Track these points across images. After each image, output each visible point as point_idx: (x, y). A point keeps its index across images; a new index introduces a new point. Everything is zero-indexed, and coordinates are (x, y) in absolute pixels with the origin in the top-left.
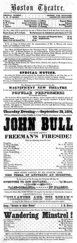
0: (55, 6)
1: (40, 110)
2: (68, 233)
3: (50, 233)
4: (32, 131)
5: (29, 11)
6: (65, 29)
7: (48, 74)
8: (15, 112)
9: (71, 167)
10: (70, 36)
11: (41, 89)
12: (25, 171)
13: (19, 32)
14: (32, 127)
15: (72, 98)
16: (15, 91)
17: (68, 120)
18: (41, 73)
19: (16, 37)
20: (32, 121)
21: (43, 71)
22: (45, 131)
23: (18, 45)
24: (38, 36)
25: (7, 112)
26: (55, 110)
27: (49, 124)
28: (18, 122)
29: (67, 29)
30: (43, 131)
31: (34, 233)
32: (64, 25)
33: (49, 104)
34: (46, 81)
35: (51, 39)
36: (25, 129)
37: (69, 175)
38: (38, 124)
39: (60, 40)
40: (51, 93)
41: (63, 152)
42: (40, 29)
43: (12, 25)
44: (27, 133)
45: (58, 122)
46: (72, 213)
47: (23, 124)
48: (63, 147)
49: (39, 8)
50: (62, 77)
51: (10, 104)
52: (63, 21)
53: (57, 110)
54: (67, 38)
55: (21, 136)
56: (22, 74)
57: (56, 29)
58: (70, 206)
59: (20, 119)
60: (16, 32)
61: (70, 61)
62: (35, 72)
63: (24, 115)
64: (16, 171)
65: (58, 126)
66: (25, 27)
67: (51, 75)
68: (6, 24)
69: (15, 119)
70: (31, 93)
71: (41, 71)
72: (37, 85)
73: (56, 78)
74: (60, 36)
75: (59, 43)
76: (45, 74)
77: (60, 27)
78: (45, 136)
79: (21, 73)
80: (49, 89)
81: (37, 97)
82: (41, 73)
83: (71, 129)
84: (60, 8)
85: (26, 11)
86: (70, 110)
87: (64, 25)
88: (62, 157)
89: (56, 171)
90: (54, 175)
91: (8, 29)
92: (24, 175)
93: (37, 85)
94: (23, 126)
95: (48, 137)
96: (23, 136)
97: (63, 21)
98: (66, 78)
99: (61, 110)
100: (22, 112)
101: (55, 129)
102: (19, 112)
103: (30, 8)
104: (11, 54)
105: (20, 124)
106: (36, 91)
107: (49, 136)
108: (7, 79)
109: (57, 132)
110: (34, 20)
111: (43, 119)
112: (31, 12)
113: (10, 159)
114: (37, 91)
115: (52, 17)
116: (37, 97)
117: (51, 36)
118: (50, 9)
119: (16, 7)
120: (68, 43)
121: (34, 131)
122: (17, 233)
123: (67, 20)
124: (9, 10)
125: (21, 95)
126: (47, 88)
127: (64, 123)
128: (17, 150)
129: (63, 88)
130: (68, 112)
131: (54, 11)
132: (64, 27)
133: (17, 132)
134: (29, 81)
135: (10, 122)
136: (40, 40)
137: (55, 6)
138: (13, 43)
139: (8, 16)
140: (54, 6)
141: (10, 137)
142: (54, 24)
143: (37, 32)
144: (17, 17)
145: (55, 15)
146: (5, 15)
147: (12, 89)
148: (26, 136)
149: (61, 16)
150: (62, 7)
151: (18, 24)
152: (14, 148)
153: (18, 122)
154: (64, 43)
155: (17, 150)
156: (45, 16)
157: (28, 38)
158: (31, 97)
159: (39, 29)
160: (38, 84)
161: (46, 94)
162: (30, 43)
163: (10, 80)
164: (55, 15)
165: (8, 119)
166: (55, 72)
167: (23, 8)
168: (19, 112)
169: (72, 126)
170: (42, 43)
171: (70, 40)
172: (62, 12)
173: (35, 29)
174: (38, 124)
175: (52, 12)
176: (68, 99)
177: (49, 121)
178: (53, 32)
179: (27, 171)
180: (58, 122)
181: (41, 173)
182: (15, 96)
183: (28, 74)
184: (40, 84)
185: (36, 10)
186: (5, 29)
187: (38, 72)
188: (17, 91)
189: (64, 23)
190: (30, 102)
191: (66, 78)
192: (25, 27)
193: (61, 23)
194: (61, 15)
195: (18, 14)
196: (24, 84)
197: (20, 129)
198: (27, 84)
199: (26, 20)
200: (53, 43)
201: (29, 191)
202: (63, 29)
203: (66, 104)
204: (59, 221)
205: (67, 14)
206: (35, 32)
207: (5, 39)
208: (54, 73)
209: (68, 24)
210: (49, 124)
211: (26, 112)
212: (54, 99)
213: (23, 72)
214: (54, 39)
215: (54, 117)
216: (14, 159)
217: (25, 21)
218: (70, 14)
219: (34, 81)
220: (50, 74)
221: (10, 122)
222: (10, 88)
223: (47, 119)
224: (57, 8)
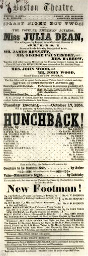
1: (50, 104)
5: (34, 12)
26: (62, 104)
39: (70, 93)
47: (7, 120)
49: (46, 8)
53: (64, 104)
58: (82, 241)
84: (69, 8)
85: (30, 12)
86: (81, 104)
118: (57, 9)
131: (62, 12)
136: (46, 94)
139: (9, 17)
145: (64, 16)
149: (70, 17)
167: (27, 7)
171: (80, 94)
172: (72, 12)
180: (35, 36)
185: (41, 10)
204: (70, 155)
205: (77, 15)
224: (65, 9)
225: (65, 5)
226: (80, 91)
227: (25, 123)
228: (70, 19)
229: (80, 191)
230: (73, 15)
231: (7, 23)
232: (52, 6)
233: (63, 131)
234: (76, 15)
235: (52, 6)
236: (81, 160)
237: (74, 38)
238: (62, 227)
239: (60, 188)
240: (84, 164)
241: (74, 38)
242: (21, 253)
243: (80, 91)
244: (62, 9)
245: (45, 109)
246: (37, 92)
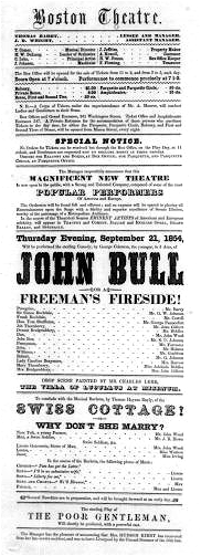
2: (172, 497)
3: (127, 496)
4: (85, 286)
5: (78, 26)
6: (164, 70)
7: (122, 145)
8: (43, 238)
9: (178, 370)
10: (175, 85)
11: (108, 182)
12: (68, 377)
13: (52, 77)
14: (86, 276)
15: (181, 205)
16: (43, 188)
17: (173, 257)
18: (105, 141)
19: (45, 90)
20: (86, 261)
21: (110, 137)
22: (117, 287)
23: (50, 108)
24: (98, 86)
25: (25, 239)
27: (128, 268)
28: (52, 263)
29: (167, 70)
30: (113, 286)
31: (88, 495)
32: (161, 58)
33: (126, 221)
34: (118, 160)
35: (130, 94)
36: (69, 281)
37: (175, 389)
38: (101, 269)
40: (132, 193)
41: (160, 331)
42: (105, 70)
43: (35, 60)
44: (73, 290)
45: (148, 263)
47: (63, 269)
48: (161, 318)
49: (102, 19)
50: (158, 151)
51: (33, 221)
52: (158, 50)
55: (58, 298)
56: (60, 145)
57: (141, 70)
59: (58, 256)
60: (46, 76)
61: (178, 103)
62: (91, 138)
63: (70, 247)
64: (48, 377)
65: (148, 274)
66: (68, 63)
67: (131, 148)
68: (22, 56)
69: (46, 255)
70: (83, 193)
71: (106, 137)
72: (96, 171)
73: (142, 154)
74: (152, 85)
75: (149, 104)
76: (116, 145)
77: (153, 63)
78: (117, 299)
79: (58, 141)
80: (124, 181)
81: (98, 202)
82: (105, 141)
83: (180, 282)
84: (150, 18)
87: (161, 58)
88: (157, 344)
89: (143, 379)
90: (140, 390)
91: (27, 71)
92: (67, 386)
93: (96, 171)
94: (63, 273)
95: (123, 301)
96: (64, 298)
97: (158, 50)
98: (166, 152)
99: (153, 233)
100: (64, 238)
101: (142, 281)
102: (54, 238)
103: (78, 17)
104: (34, 128)
105: (57, 268)
106: (95, 188)
107: (128, 299)
108: (23, 158)
109: (147, 288)
110: (89, 47)
111: (112, 255)
113: (32, 348)
114: (99, 188)
115: (133, 39)
116: (98, 202)
117: (131, 86)
118: (127, 19)
119: (46, 15)
120: (171, 103)
121: (89, 286)
122: (50, 495)
123: (167, 47)
124: (28, 23)
125: (57, 199)
126: (122, 179)
127: (164, 266)
128: (47, 326)
129: (160, 178)
130: (171, 238)
131: (137, 26)
132: (160, 63)
133: (50, 288)
134: (78, 161)
135: (32, 263)
136: (104, 97)
137: (139, 13)
138: (38, 104)
140: (135, 12)
141: (33, 299)
142: (135, 56)
143: (95, 76)
144: (48, 39)
145: (140, 34)
146: (20, 36)
147: (37, 182)
148: (70, 299)
149: (153, 37)
150: (181, 408)
151: (51, 57)
152: (42, 324)
153: (52, 263)
154: (162, 103)
155: (47, 326)
156: (114, 38)
157: (75, 91)
158: (83, 202)
159: (101, 70)
160: (99, 168)
161: (120, 196)
162: (79, 103)
163: (31, 160)
164: (140, 34)
165: (26, 256)
166: (141, 138)
167: (63, 17)
168: (54, 238)
169: (182, 273)
170: (109, 103)
171: (175, 96)
173: (91, 70)
174: (101, 269)
175: (132, 27)
176: (173, 207)
177: (128, 262)
178: (134, 76)
179: (74, 378)
180: (148, 263)
181: (107, 384)
182: (44, 199)
183: (73, 145)
184: (104, 169)
185: (92, 21)
186: (20, 71)
187: (99, 139)
188: (49, 188)
189: (161, 54)
190: (81, 216)
191: (166, 152)
192: (68, 63)
193: (154, 54)
194: (153, 34)
195: (50, 33)
196: (65, 169)
197: (57, 281)
198: (73, 169)
199: (71, 47)
200: (135, 104)
202: (158, 70)
203: (168, 222)
205: (168, 33)
206: (91, 76)
207: (21, 94)
208: (137, 141)
209: (172, 58)
210: (128, 268)
211: (75, 239)
212: (137, 207)
213: (64, 140)
214: (139, 94)
215: (139, 251)
216: (42, 346)
217: (67, 50)
218: (175, 33)
219: (88, 160)
220: (128, 144)
221: (32, 263)
222: (33, 178)
223: (122, 255)
225: (143, 12)
226: (175, 90)
231: (64, 140)
233: (124, 118)
234: (165, 33)
238: (169, 361)
239: (158, 296)
242: (40, 168)
243: (175, 90)
245: (82, 49)
246: (86, 92)
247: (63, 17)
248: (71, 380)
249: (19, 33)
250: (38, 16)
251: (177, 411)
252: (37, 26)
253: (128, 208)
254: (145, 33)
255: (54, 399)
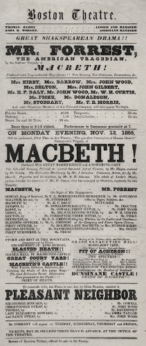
0: (101, 12)
37: (133, 92)
46: (134, 147)
49: (74, 16)
54: (127, 115)
75: (81, 339)
85: (52, 21)
112: (61, 21)
118: (92, 16)
119: (36, 13)
137: (101, 12)
164: (110, 26)
167: (48, 15)
172: (113, 21)
185: (68, 17)
201: (30, 167)
225: (103, 11)
227: (11, 159)
228: (119, 27)
229: (134, 161)
230: (122, 25)
232: (84, 14)
234: (127, 26)
235: (84, 14)
236: (133, 227)
237: (53, 296)
240: (138, 235)
241: (53, 296)
244: (98, 17)
247: (48, 15)
248: (38, 287)
249: (8, 25)
250: (31, 14)
251: (135, 274)
252: (30, 20)
253: (72, 323)
254: (113, 25)
255: (65, 169)
